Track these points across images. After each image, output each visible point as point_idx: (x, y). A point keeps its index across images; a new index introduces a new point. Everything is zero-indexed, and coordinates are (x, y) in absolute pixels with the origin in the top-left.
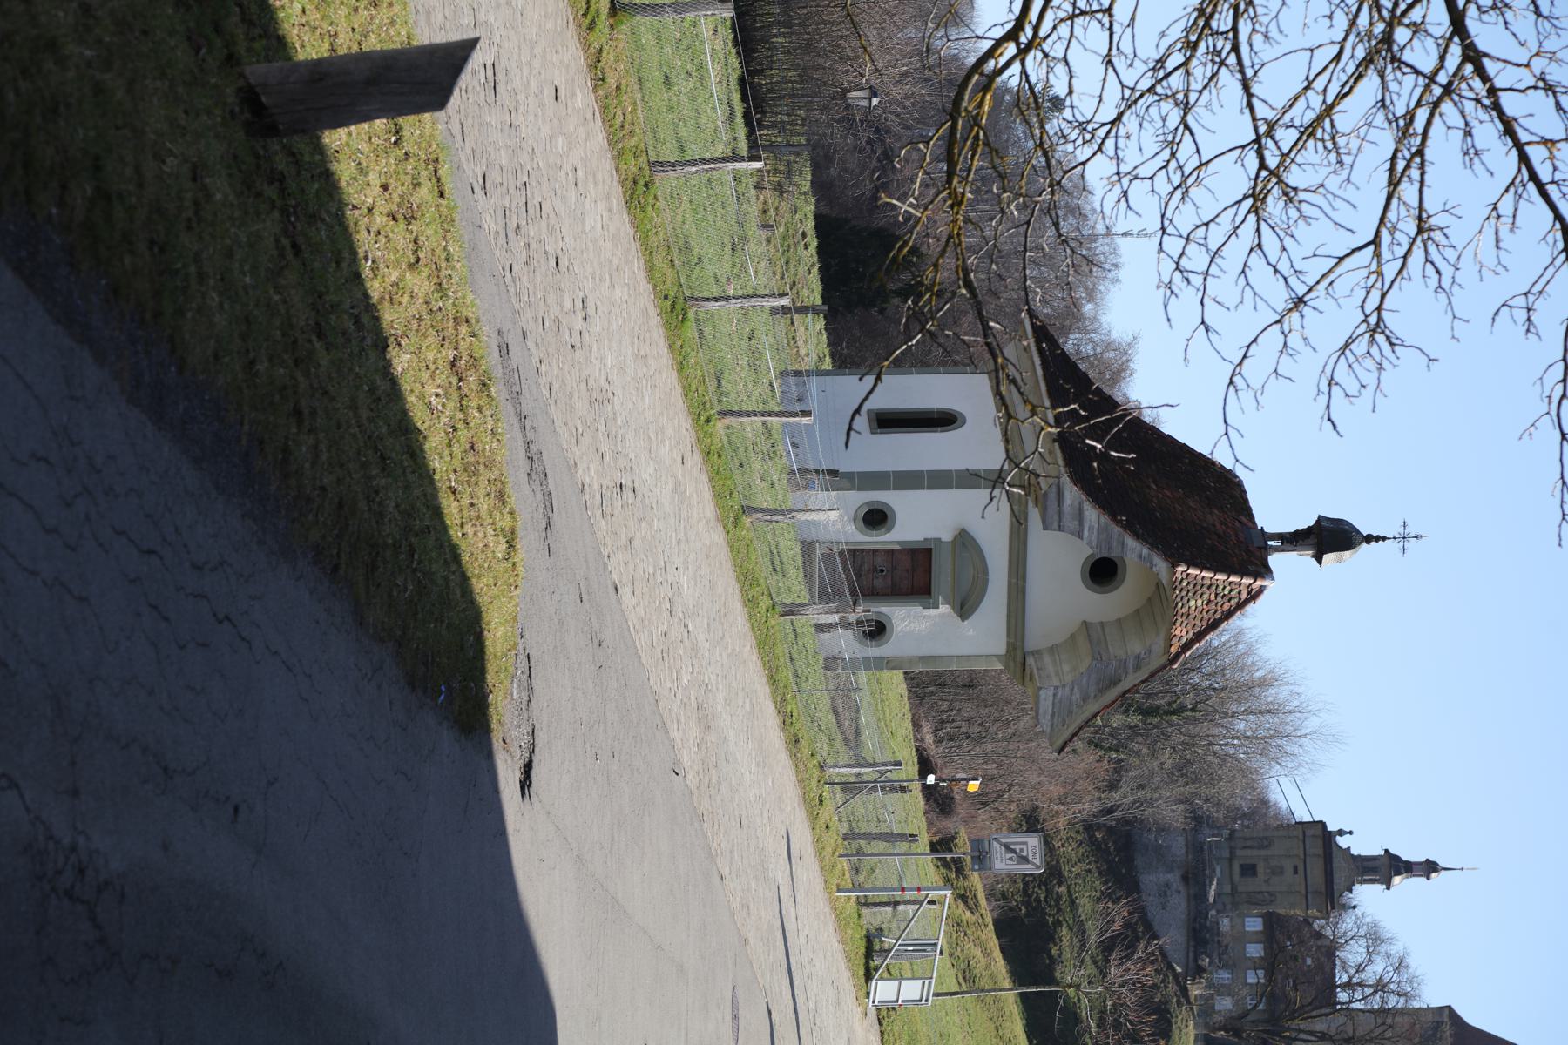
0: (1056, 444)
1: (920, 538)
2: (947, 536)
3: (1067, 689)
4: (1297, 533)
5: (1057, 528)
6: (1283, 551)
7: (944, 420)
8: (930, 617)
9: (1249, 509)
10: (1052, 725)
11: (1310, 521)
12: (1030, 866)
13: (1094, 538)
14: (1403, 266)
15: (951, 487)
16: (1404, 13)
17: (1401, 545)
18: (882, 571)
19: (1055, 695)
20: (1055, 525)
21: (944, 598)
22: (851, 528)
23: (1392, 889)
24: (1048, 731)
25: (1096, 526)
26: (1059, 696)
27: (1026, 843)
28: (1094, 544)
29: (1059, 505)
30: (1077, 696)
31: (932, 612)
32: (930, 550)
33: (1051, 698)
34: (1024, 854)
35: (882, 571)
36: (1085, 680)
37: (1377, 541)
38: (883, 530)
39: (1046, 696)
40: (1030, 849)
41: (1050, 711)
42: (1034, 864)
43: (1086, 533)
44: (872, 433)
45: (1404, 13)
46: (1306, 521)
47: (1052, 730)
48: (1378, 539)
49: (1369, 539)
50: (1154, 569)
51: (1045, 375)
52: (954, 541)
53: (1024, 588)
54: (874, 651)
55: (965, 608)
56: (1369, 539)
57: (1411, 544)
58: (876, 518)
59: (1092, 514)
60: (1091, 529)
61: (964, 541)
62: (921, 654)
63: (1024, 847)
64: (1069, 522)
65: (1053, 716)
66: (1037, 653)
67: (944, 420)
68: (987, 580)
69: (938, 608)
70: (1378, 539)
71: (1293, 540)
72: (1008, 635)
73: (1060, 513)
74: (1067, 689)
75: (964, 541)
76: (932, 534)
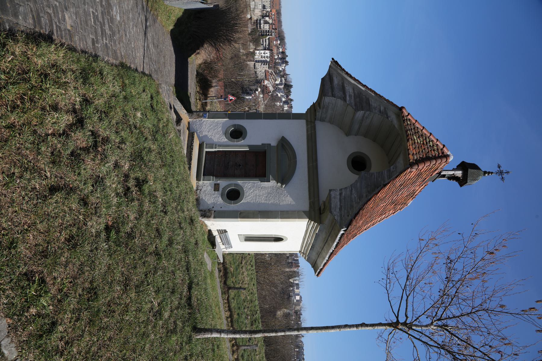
1: (260, 143)
2: (274, 143)
3: (348, 190)
5: (331, 95)
7: (249, 239)
8: (265, 188)
10: (341, 215)
13: (353, 101)
16: (351, 191)
18: (240, 165)
20: (330, 94)
22: (224, 140)
24: (339, 220)
26: (343, 194)
28: (353, 104)
29: (331, 84)
30: (355, 195)
33: (338, 197)
35: (240, 165)
37: (454, 169)
38: (240, 139)
45: (351, 191)
47: (341, 219)
50: (389, 119)
54: (233, 206)
60: (350, 96)
62: (260, 210)
65: (340, 209)
67: (249, 239)
68: (296, 161)
69: (270, 182)
74: (348, 190)
75: (284, 143)
76: (266, 142)
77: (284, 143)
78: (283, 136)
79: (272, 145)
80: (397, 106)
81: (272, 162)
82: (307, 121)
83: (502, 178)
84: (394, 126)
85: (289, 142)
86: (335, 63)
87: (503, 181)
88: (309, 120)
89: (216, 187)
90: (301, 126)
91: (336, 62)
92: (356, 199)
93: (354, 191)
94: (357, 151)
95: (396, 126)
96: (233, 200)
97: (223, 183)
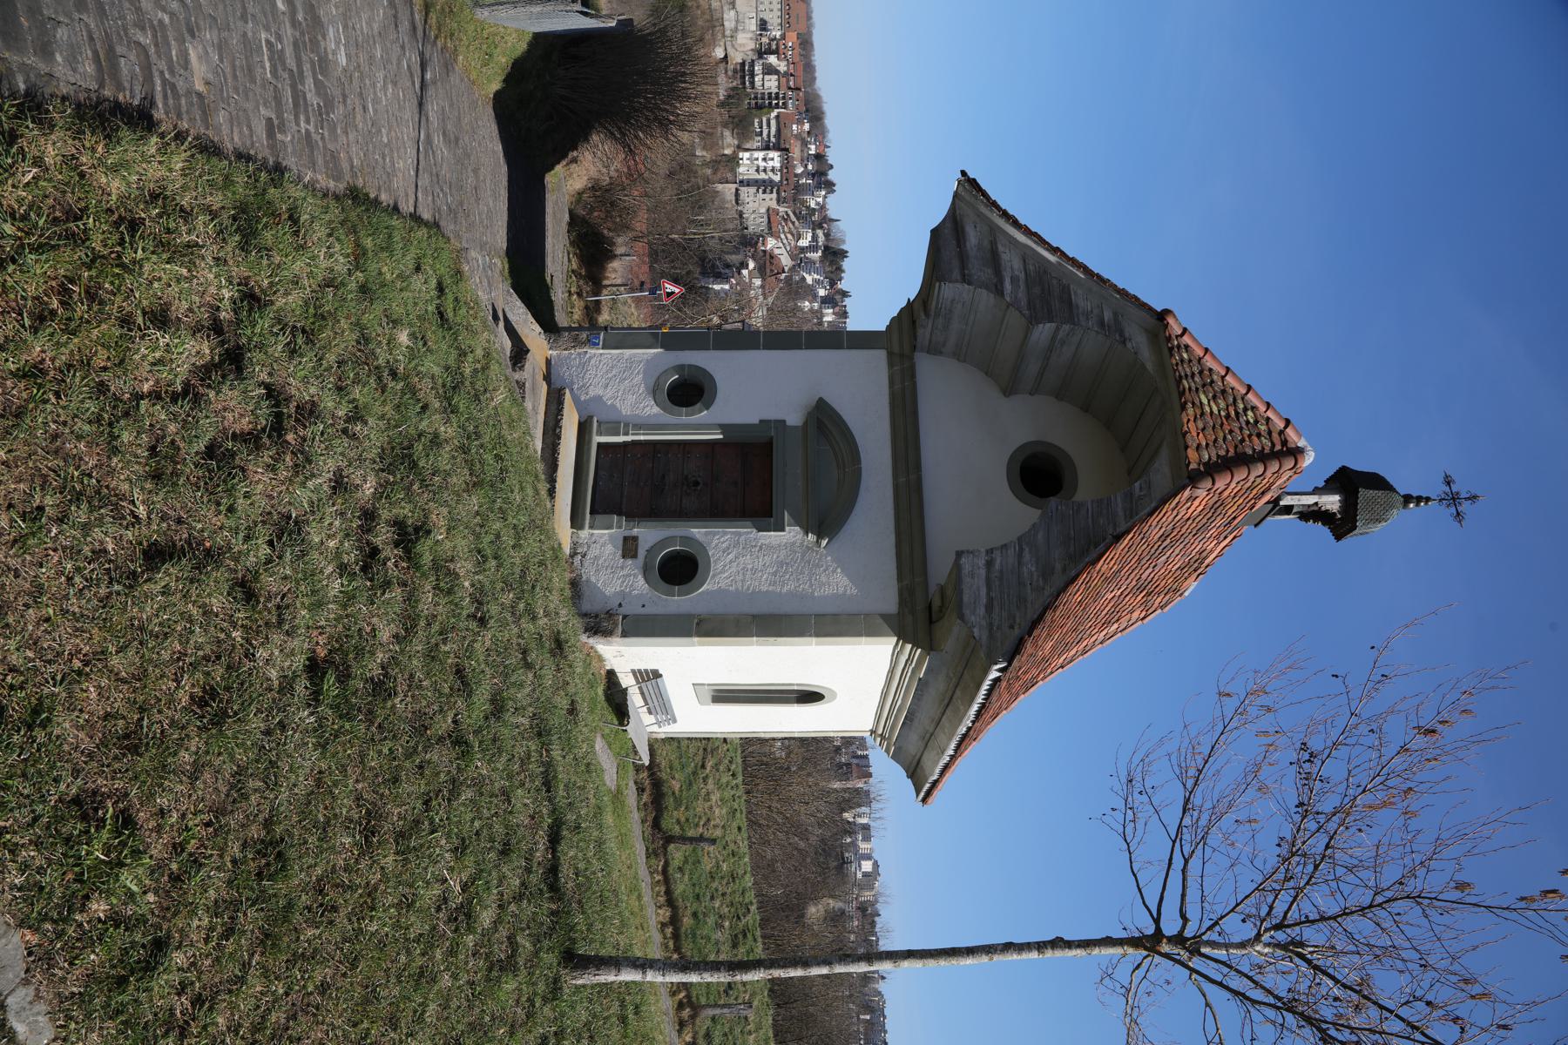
1: (752, 418)
2: (794, 419)
3: (1011, 552)
8: (770, 547)
10: (991, 625)
13: (1022, 294)
14: (1126, 840)
15: (800, 348)
18: (697, 483)
20: (956, 274)
21: (790, 514)
25: (1022, 276)
26: (997, 566)
28: (1024, 303)
29: (959, 246)
30: (1030, 567)
31: (772, 537)
33: (983, 572)
35: (697, 483)
36: (1040, 536)
38: (698, 405)
41: (984, 600)
43: (1008, 286)
47: (991, 636)
50: (1129, 345)
54: (677, 602)
60: (1014, 280)
62: (755, 611)
65: (989, 607)
72: (900, 578)
74: (1011, 552)
75: (823, 419)
77: (823, 419)
78: (821, 399)
79: (788, 423)
80: (1150, 309)
81: (789, 472)
82: (890, 355)
83: (1458, 514)
84: (1143, 366)
85: (832, 409)
86: (969, 184)
87: (1460, 521)
88: (896, 349)
89: (629, 548)
90: (875, 363)
91: (973, 183)
92: (1035, 577)
93: (1027, 556)
94: (1033, 439)
95: (1149, 366)
96: (679, 584)
97: (649, 534)
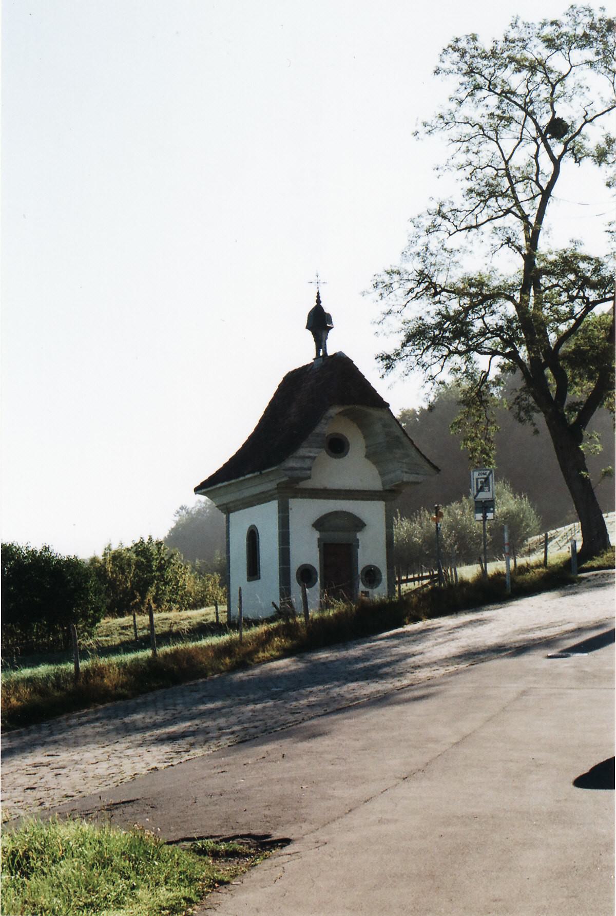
0: (263, 472)
4: (211, 478)
6: (326, 348)
7: (253, 536)
9: (304, 367)
11: (309, 333)
12: (490, 477)
17: (322, 285)
19: (406, 472)
20: (308, 472)
23: (584, 241)
26: (406, 470)
27: (477, 479)
32: (325, 545)
34: (483, 480)
37: (321, 302)
39: (406, 478)
40: (480, 477)
42: (489, 474)
44: (260, 578)
46: (309, 336)
48: (318, 297)
49: (318, 301)
51: (227, 481)
52: (320, 531)
53: (346, 491)
55: (358, 524)
56: (318, 301)
57: (322, 278)
58: (306, 574)
59: (303, 451)
61: (319, 524)
63: (479, 480)
64: (308, 463)
66: (384, 484)
67: (253, 536)
70: (318, 297)
71: (320, 343)
73: (302, 469)
75: (319, 524)
76: (316, 544)
